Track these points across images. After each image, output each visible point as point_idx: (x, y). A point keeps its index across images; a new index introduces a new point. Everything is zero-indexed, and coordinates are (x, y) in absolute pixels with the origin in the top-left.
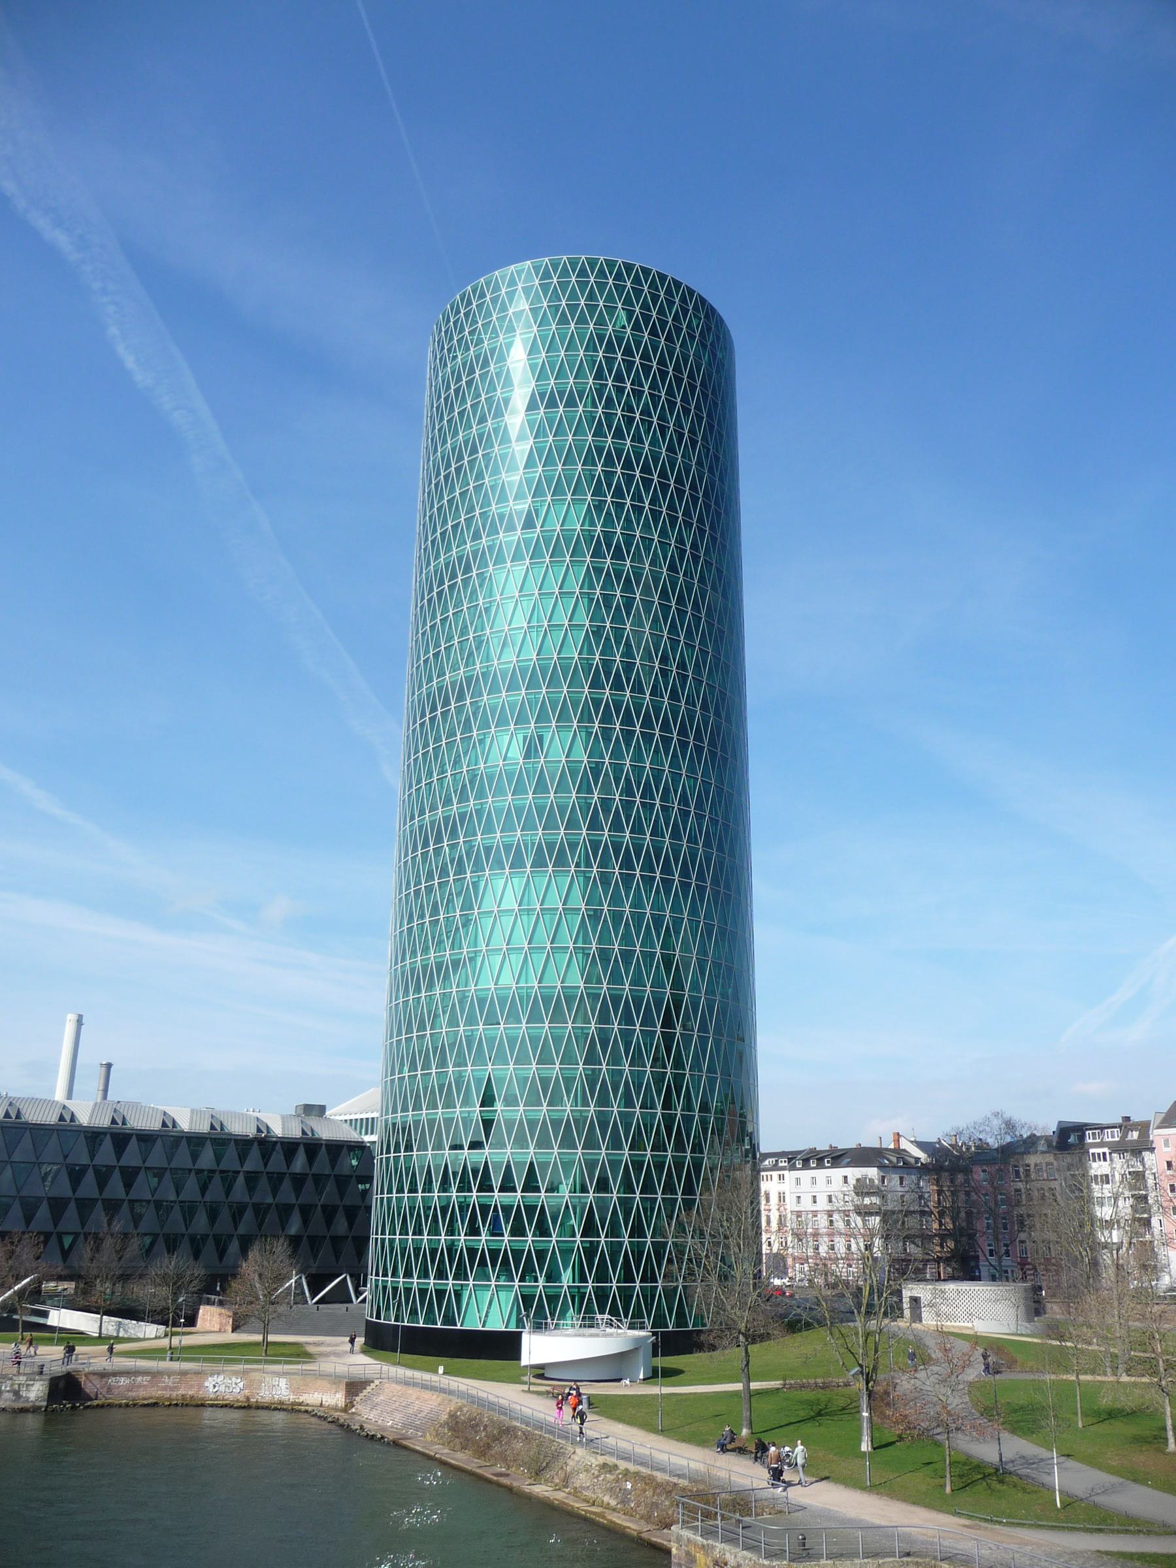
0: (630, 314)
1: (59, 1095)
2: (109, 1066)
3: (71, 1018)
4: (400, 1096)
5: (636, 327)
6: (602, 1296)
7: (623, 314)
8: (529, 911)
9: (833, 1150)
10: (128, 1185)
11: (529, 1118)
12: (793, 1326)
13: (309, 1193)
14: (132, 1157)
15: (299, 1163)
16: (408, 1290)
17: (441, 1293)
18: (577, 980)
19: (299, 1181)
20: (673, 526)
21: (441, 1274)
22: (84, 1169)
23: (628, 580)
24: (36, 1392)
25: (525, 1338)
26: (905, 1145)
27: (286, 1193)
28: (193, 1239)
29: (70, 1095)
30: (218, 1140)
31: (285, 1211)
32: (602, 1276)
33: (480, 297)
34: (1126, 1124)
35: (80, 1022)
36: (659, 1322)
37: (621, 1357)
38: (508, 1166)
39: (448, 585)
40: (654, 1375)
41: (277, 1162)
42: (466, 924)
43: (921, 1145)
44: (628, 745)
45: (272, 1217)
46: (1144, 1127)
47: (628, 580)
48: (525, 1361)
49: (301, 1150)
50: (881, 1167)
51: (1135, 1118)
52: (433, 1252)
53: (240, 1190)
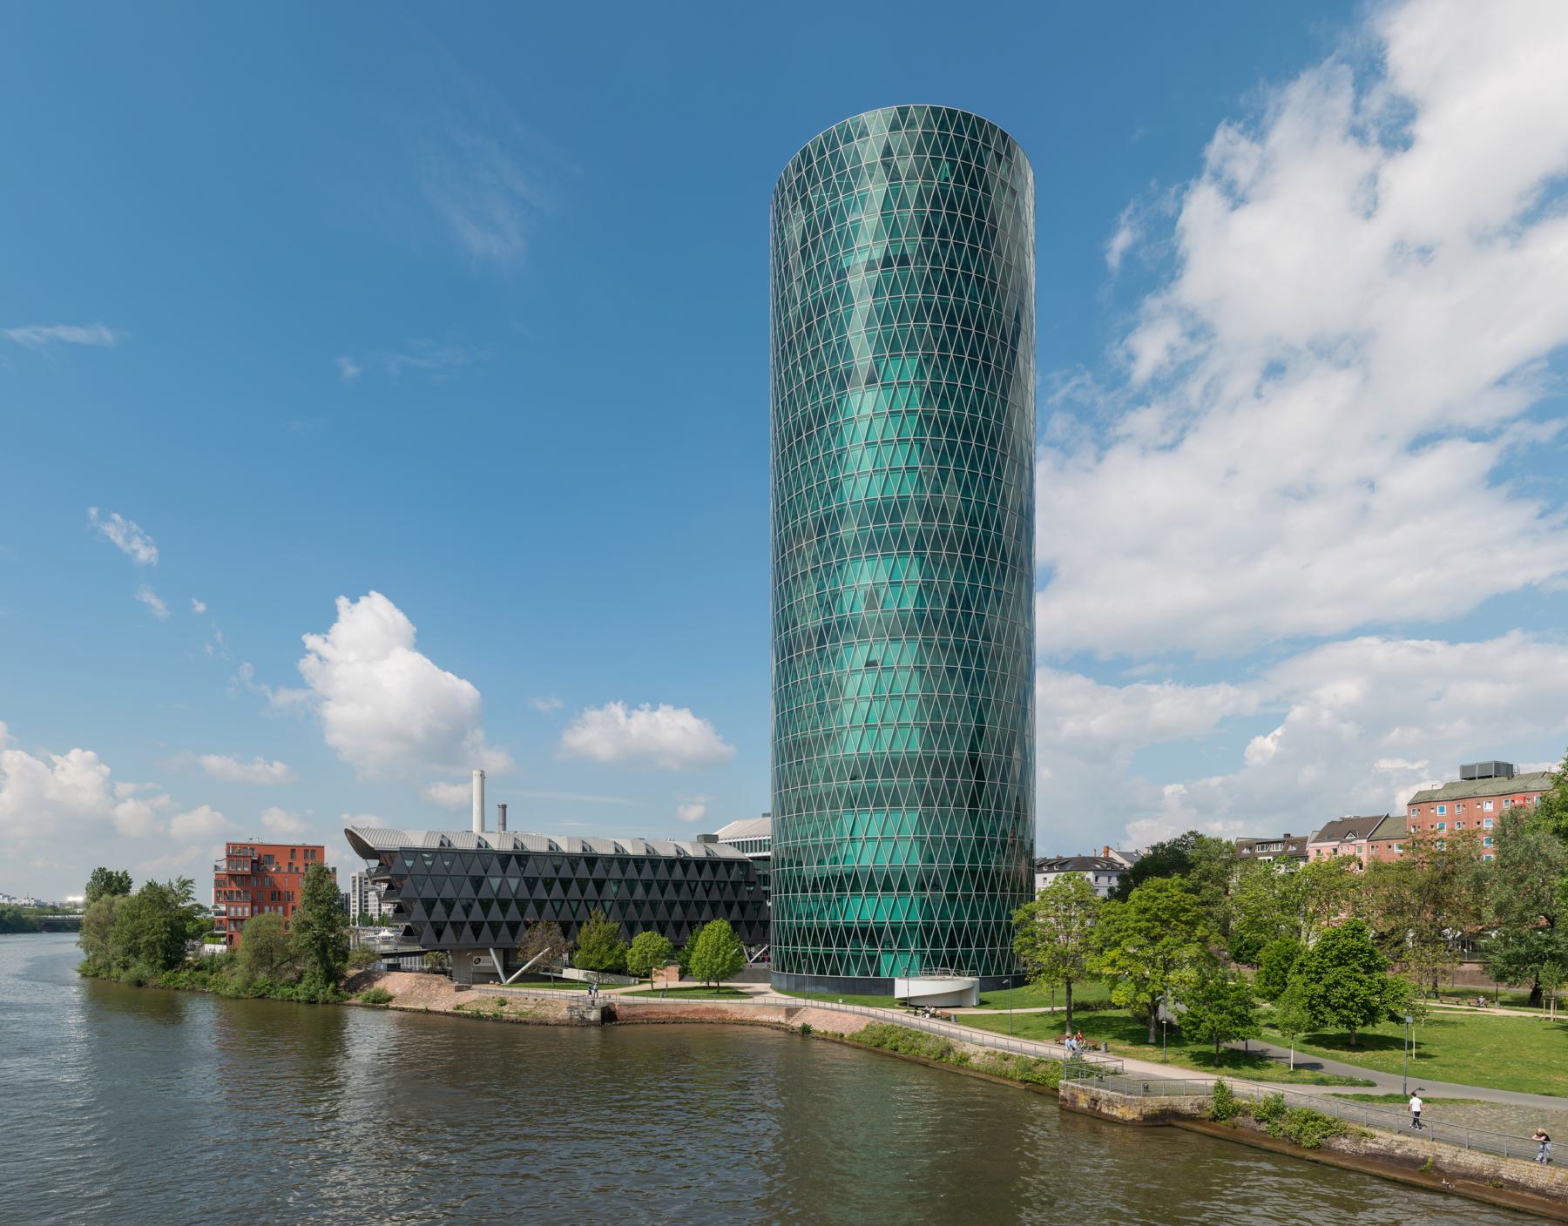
0: (953, 164)
1: (476, 829)
2: (504, 807)
3: (476, 773)
4: (782, 828)
5: (959, 180)
6: (936, 956)
7: (947, 165)
8: (881, 698)
9: (1060, 858)
10: (707, 893)
11: (883, 840)
12: (24, 1051)
13: (670, 894)
14: (599, 872)
15: (678, 873)
16: (795, 954)
17: (828, 956)
18: (916, 747)
19: (678, 885)
20: (974, 370)
21: (815, 944)
22: (553, 880)
23: (951, 426)
24: (594, 1015)
25: (897, 981)
26: (1112, 854)
27: (670, 894)
28: (659, 924)
29: (483, 830)
30: (651, 861)
31: (729, 906)
32: (936, 944)
33: (840, 168)
34: (1287, 840)
35: (482, 776)
36: (987, 971)
37: (961, 993)
38: (887, 877)
39: (805, 433)
40: (982, 1003)
41: (662, 873)
42: (834, 709)
43: (1122, 855)
44: (952, 567)
45: (722, 907)
46: (1302, 842)
47: (951, 426)
48: (897, 995)
49: (707, 866)
50: (1095, 870)
51: (1295, 835)
52: (809, 930)
53: (700, 894)
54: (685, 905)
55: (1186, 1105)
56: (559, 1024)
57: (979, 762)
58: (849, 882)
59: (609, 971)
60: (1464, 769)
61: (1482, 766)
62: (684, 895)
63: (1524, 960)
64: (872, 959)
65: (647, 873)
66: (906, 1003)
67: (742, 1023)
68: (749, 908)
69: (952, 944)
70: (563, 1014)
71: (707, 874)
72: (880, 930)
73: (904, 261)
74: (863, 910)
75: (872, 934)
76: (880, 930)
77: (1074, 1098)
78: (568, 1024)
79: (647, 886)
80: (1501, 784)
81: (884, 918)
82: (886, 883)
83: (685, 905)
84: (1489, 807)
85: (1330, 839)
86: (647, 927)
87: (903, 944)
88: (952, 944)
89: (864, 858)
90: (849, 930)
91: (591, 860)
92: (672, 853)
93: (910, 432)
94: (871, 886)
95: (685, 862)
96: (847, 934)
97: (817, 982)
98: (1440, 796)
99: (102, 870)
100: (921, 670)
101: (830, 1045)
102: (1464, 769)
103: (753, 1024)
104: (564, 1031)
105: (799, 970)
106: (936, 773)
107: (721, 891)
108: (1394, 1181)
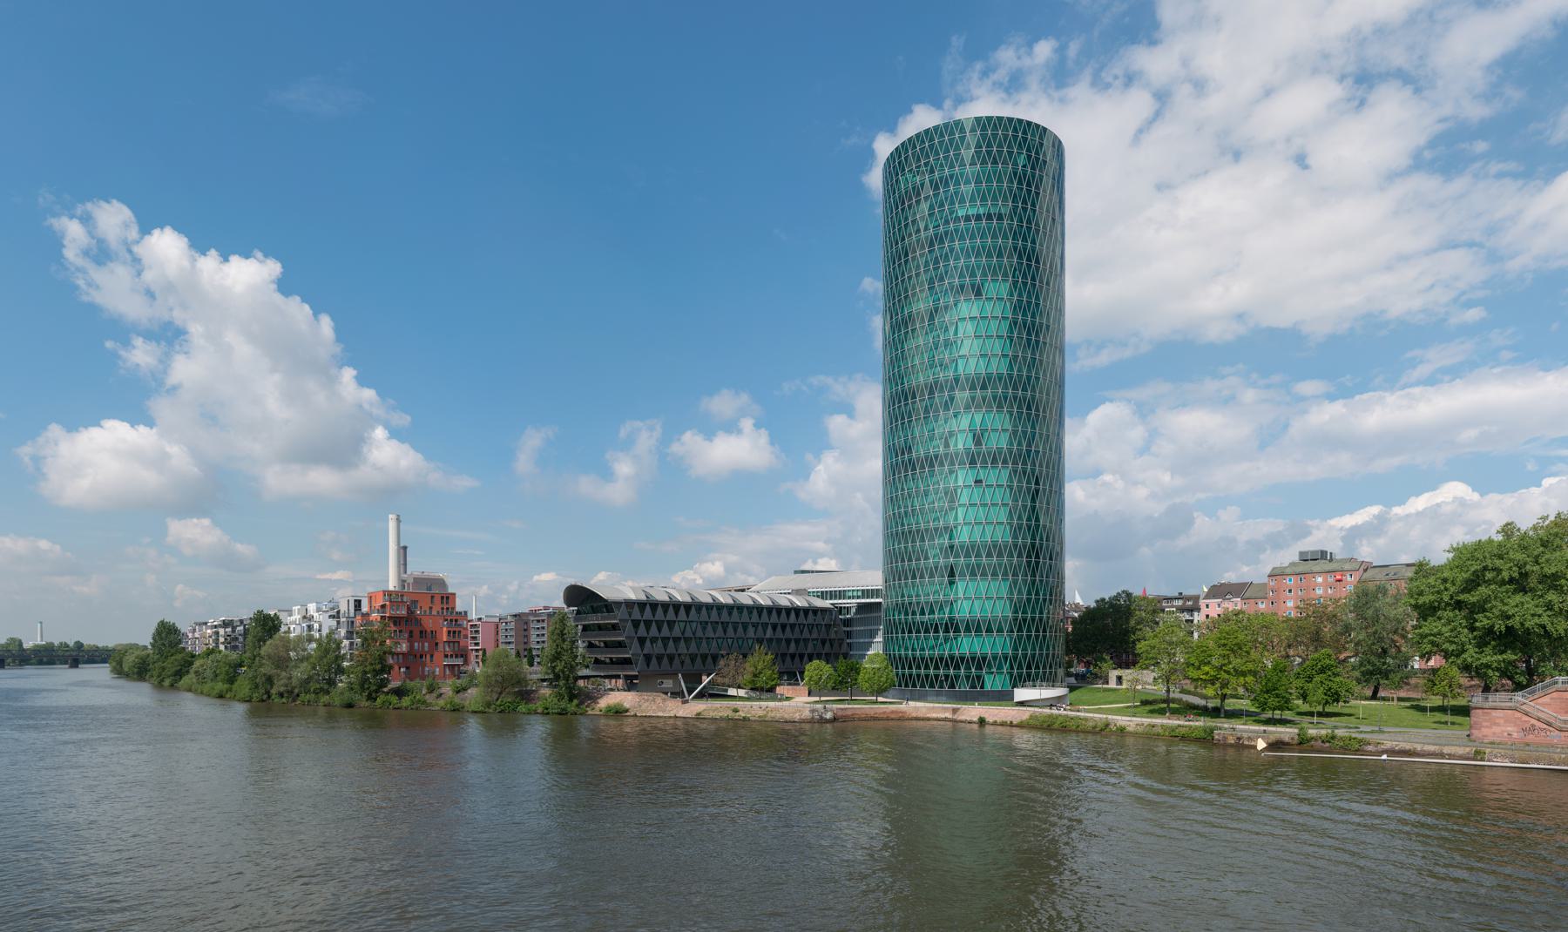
2: (405, 548)
35: (398, 520)
41: (745, 617)
46: (1196, 599)
54: (797, 641)
55: (1286, 739)
56: (803, 721)
57: (1036, 549)
58: (952, 626)
59: (762, 689)
60: (1301, 553)
61: (1313, 552)
62: (797, 635)
63: (1371, 673)
64: (979, 677)
65: (774, 618)
66: (1022, 704)
67: (917, 719)
68: (836, 645)
69: (1029, 667)
70: (807, 714)
71: (735, 617)
72: (984, 659)
73: (1000, 218)
74: (966, 645)
75: (980, 662)
76: (984, 659)
77: (1225, 738)
78: (811, 721)
79: (774, 627)
80: (1322, 565)
81: (988, 650)
82: (975, 627)
83: (797, 641)
84: (1320, 580)
85: (1214, 597)
86: (819, 657)
87: (1000, 667)
88: (1029, 667)
89: (964, 610)
90: (962, 659)
91: (654, 605)
92: (666, 598)
93: (1004, 332)
94: (978, 630)
95: (720, 607)
96: (956, 661)
97: (938, 694)
98: (1289, 571)
99: (260, 612)
100: (1011, 488)
101: (1015, 730)
102: (1301, 553)
103: (929, 719)
104: (807, 726)
105: (914, 686)
106: (1020, 555)
107: (648, 629)
108: (1423, 756)
